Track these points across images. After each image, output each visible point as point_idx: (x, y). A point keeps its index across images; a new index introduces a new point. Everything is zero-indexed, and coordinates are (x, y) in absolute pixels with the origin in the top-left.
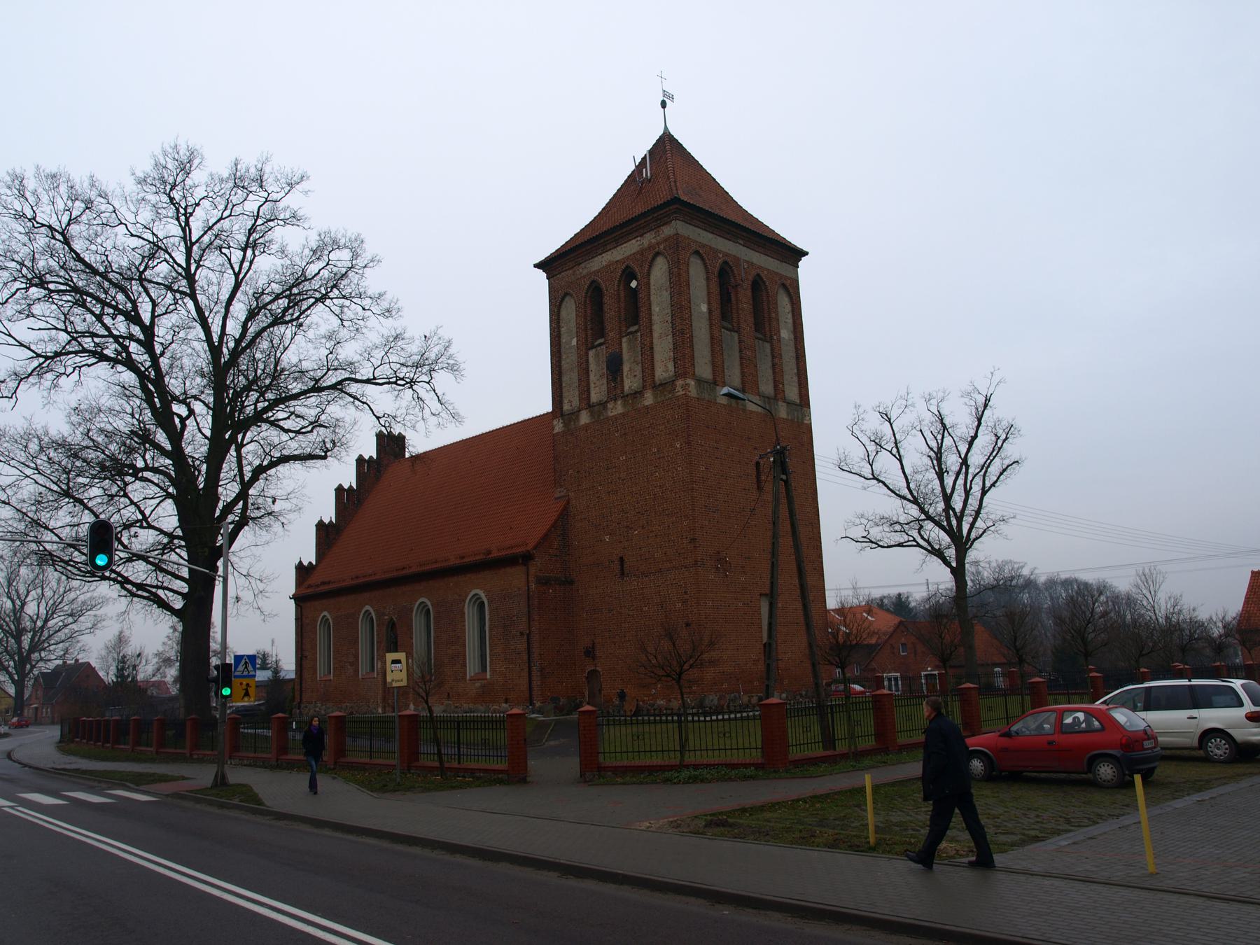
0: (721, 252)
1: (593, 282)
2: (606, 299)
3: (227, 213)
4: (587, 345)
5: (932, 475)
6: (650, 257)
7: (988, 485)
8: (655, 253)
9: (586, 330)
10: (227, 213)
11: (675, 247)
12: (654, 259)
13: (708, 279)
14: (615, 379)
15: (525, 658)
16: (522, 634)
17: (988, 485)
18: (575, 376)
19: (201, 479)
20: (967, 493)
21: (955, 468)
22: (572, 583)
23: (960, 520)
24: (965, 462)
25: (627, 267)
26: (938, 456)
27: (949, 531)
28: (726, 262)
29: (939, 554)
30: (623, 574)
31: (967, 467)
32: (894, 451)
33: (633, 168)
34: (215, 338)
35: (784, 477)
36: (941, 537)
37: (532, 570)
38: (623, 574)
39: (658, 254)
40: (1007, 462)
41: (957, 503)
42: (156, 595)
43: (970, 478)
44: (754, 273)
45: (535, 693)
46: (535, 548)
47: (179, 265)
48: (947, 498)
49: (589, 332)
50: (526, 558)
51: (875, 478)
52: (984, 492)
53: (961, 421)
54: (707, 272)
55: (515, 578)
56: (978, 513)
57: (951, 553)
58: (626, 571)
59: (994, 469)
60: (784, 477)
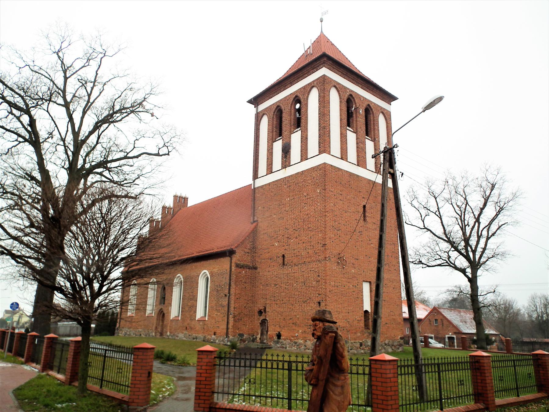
0: (348, 89)
1: (278, 106)
2: (284, 115)
3: (87, 64)
4: (271, 141)
5: (457, 228)
6: (309, 89)
7: (490, 234)
8: (311, 86)
9: (272, 132)
10: (87, 64)
11: (323, 85)
12: (310, 90)
13: (341, 102)
14: (286, 157)
15: (226, 309)
16: (226, 295)
17: (490, 234)
18: (287, 380)
19: (61, 203)
20: (479, 237)
21: (471, 223)
22: (256, 268)
23: (474, 252)
24: (478, 220)
25: (296, 96)
26: (462, 218)
27: (467, 257)
28: (351, 95)
29: (463, 271)
30: (284, 264)
31: (479, 223)
32: (437, 213)
33: (304, 52)
34: (76, 130)
35: (392, 171)
36: (462, 262)
37: (234, 260)
38: (284, 264)
39: (313, 87)
40: (501, 224)
41: (473, 242)
42: (28, 262)
43: (481, 229)
44: (367, 103)
45: (230, 330)
46: (236, 247)
47: (59, 89)
48: (467, 240)
49: (274, 133)
50: (230, 253)
51: (425, 228)
52: (488, 238)
53: (476, 201)
54: (340, 98)
55: (224, 264)
56: (484, 249)
57: (469, 271)
58: (286, 263)
59: (494, 228)
60: (392, 171)
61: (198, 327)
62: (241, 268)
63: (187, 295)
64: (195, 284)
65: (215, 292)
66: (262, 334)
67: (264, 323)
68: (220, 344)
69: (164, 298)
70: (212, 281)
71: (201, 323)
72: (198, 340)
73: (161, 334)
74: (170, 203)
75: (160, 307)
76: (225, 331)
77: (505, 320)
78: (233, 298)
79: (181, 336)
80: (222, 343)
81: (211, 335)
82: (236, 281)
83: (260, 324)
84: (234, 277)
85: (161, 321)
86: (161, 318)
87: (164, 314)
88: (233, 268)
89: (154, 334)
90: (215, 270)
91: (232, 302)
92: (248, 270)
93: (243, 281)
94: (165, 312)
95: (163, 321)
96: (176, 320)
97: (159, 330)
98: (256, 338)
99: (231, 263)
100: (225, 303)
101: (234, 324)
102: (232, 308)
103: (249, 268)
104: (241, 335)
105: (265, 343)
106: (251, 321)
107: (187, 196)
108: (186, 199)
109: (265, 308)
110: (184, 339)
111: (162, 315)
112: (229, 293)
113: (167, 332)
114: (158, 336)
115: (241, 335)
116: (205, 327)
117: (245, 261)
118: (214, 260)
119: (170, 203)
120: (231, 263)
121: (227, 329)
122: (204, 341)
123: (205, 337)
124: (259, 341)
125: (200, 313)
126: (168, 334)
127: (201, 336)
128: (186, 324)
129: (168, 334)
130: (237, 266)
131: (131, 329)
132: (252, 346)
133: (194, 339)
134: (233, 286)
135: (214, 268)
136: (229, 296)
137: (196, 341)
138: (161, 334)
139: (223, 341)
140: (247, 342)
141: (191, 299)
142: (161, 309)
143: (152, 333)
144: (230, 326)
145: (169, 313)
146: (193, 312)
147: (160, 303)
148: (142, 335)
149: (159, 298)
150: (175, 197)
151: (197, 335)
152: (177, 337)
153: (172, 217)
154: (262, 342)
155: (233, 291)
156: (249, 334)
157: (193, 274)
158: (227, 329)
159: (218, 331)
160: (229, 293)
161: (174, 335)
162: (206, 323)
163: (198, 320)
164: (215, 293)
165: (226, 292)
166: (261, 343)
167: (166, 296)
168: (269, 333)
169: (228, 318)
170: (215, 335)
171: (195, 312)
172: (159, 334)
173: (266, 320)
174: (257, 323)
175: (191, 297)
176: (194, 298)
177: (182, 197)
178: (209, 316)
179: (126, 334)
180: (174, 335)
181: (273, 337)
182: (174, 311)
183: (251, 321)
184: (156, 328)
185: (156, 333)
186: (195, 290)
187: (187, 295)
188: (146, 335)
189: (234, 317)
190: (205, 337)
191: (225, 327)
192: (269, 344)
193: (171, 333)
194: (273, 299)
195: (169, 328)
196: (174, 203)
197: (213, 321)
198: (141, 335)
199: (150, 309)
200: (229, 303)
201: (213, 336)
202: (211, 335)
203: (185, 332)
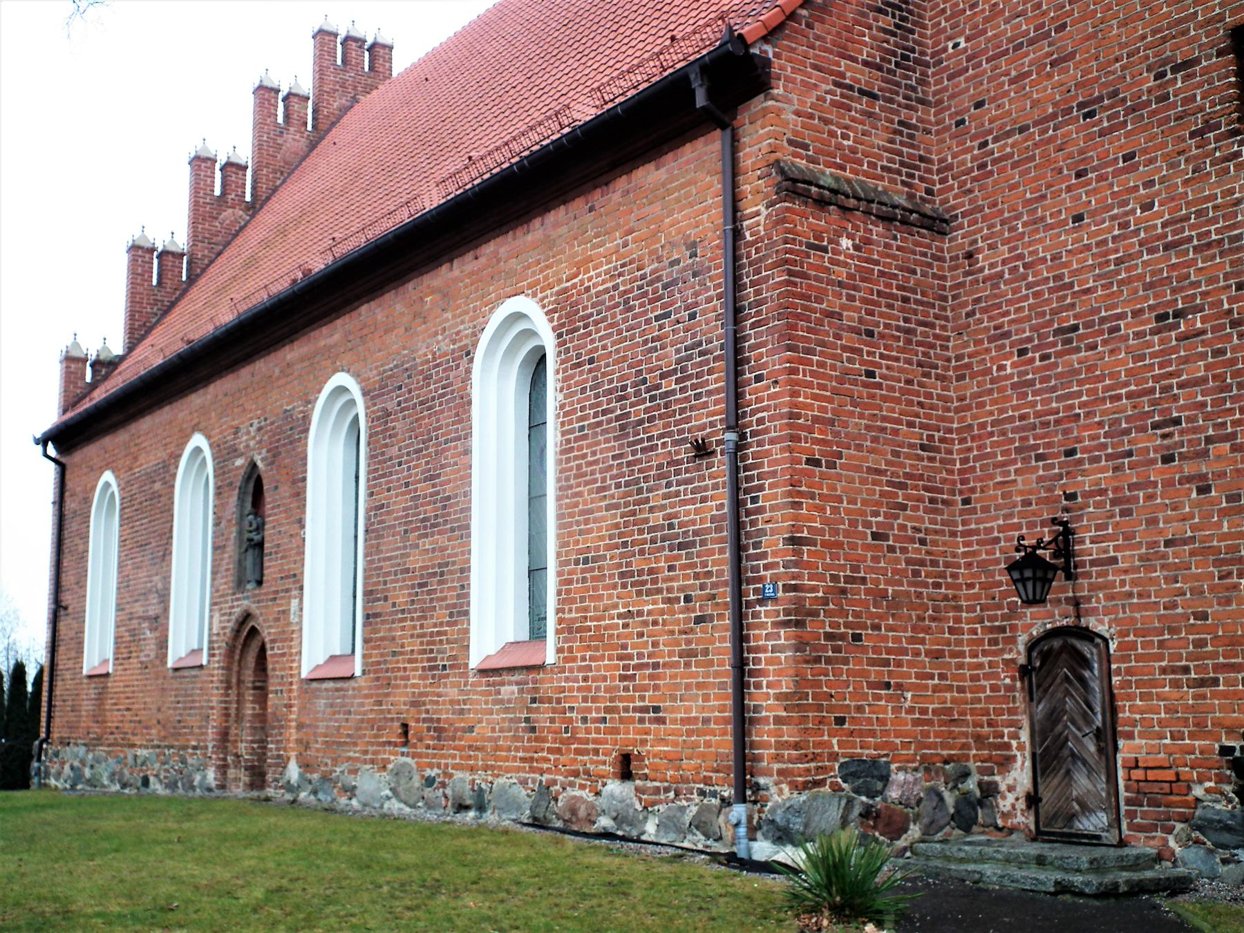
15: (719, 561)
16: (702, 450)
45: (763, 735)
46: (772, 34)
61: (490, 716)
62: (821, 203)
63: (399, 502)
64: (447, 419)
65: (610, 414)
66: (1050, 758)
67: (1060, 661)
68: (682, 855)
69: (260, 545)
70: (572, 364)
71: (509, 691)
72: (490, 817)
73: (258, 778)
74: (297, 72)
75: (244, 604)
76: (724, 742)
77: (255, 728)
78: (772, 457)
79: (372, 784)
80: (697, 840)
81: (594, 781)
82: (791, 316)
83: (1025, 671)
84: (766, 288)
85: (249, 695)
86: (249, 675)
87: (263, 649)
88: (759, 214)
89: (211, 775)
90: (596, 278)
91: (771, 498)
92: (877, 230)
93: (850, 318)
94: (268, 632)
95: (262, 692)
96: (333, 680)
97: (242, 748)
98: (989, 791)
99: (734, 172)
100: (704, 503)
101: (801, 682)
102: (771, 542)
103: (887, 219)
104: (867, 775)
105: (1093, 840)
106: (936, 655)
107: (385, 39)
108: (379, 52)
109: (1067, 532)
110: (395, 806)
111: (250, 649)
112: (735, 421)
113: (283, 764)
114: (238, 790)
115: (867, 775)
116: (543, 718)
117: (851, 157)
118: (579, 205)
119: (297, 72)
120: (734, 172)
121: (743, 721)
122: (538, 823)
123: (545, 791)
124: (1025, 819)
125: (494, 621)
126: (293, 772)
127: (513, 787)
128: (399, 700)
129: (293, 772)
130: (792, 186)
131: (101, 751)
132: (990, 871)
133: (462, 807)
134: (767, 354)
135: (582, 265)
136: (740, 446)
137: (473, 833)
138: (258, 778)
139: (699, 824)
140: (915, 831)
141: (429, 526)
142: (247, 616)
143: (201, 768)
144: (767, 698)
145: (291, 635)
146: (441, 614)
147: (240, 583)
148: (156, 786)
149: (232, 550)
150: (324, 37)
151: (480, 778)
152: (351, 791)
153: (313, 146)
154: (1053, 827)
155: (767, 400)
156: (928, 766)
157: (430, 345)
158: (743, 721)
159: (653, 749)
160: (735, 421)
161: (325, 778)
162: (548, 685)
163: (483, 672)
164: (606, 447)
165: (708, 418)
166: (1038, 835)
167: (268, 532)
168: (1126, 750)
169: (740, 637)
170: (626, 774)
171: (461, 611)
172: (245, 778)
173: (1088, 635)
174: (993, 669)
175: (429, 511)
176: (446, 517)
177: (360, 41)
178: (567, 629)
179: (77, 777)
180: (325, 778)
181: (1179, 784)
182: (323, 625)
183: (936, 655)
184: (224, 736)
185: (223, 768)
186: (449, 458)
187: (399, 502)
188: (172, 785)
189: (798, 618)
190: (545, 791)
191: (719, 705)
192: (1143, 846)
193: (306, 766)
194: (1152, 443)
195: (293, 734)
196: (321, 72)
197: (608, 667)
198: (146, 782)
199: (191, 628)
200: (737, 504)
201: (614, 787)
202: (594, 781)
203: (399, 759)
